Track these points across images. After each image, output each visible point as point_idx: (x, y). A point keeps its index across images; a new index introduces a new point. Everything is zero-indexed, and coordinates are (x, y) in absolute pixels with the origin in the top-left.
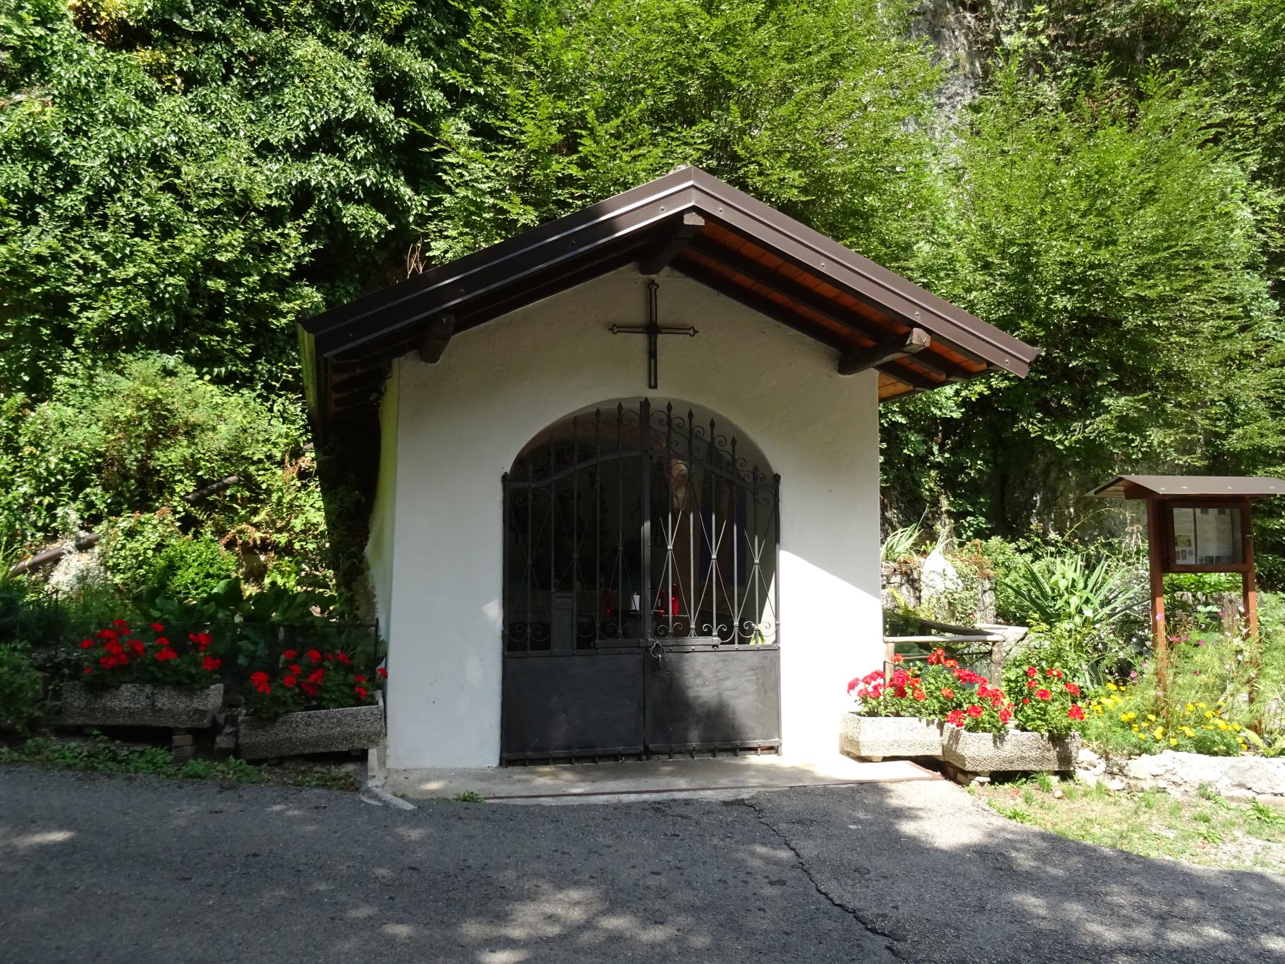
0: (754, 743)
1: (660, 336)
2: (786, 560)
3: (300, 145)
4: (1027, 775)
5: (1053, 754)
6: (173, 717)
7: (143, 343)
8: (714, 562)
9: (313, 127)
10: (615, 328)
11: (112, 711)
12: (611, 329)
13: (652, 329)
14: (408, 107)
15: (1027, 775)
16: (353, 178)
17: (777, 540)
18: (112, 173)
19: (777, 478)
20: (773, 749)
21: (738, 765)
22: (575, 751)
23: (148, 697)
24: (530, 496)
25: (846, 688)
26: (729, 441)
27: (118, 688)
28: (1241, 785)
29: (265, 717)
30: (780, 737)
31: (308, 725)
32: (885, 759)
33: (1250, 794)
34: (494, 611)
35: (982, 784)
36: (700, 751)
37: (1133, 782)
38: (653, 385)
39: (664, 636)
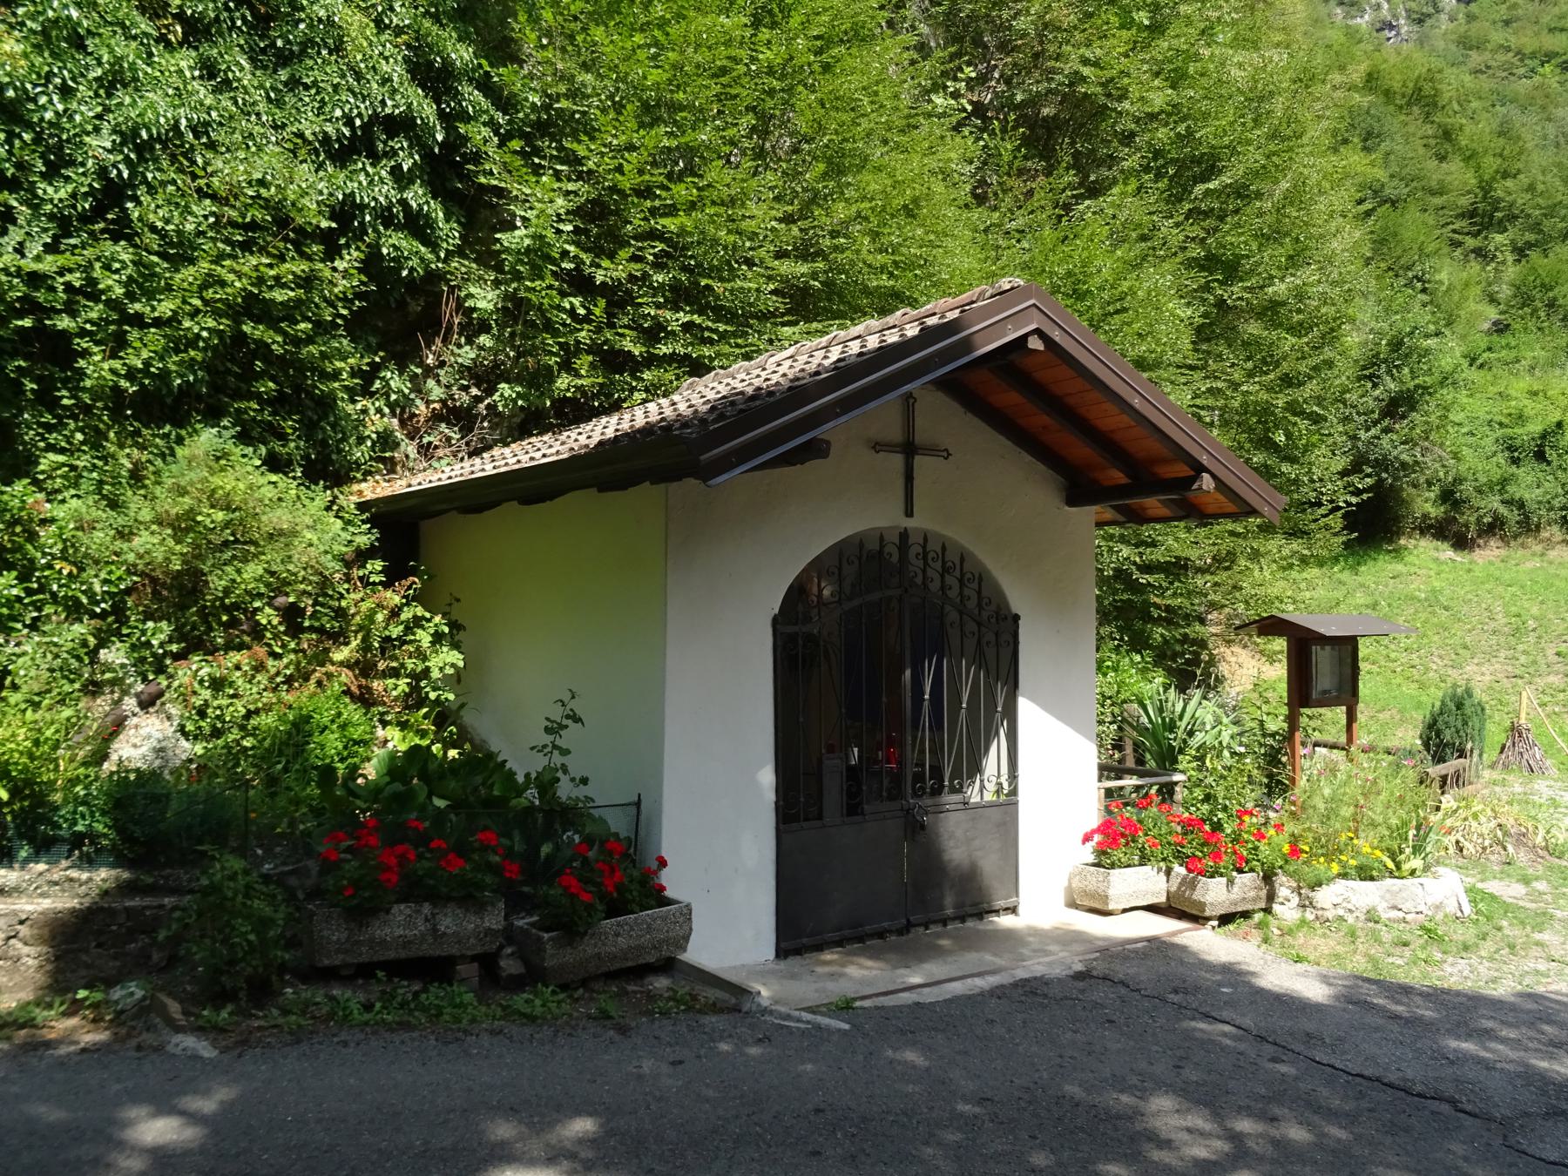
0: (1001, 903)
1: (917, 458)
2: (1026, 708)
3: (341, 144)
4: (1246, 915)
5: (1263, 893)
6: (459, 942)
7: (198, 414)
8: (926, 703)
9: (358, 122)
10: (878, 446)
11: (383, 942)
12: (874, 447)
13: (909, 449)
14: (449, 105)
15: (1246, 915)
16: (394, 196)
17: (1016, 686)
18: (127, 160)
19: (1016, 618)
20: (1013, 910)
21: (978, 931)
22: (847, 932)
23: (427, 920)
24: (800, 642)
25: (1081, 837)
26: (977, 576)
27: (388, 912)
28: (1395, 907)
29: (570, 928)
30: (1017, 896)
31: (617, 935)
32: (1125, 911)
33: (1401, 914)
34: (767, 777)
35: (1213, 928)
36: (954, 919)
37: (1320, 913)
38: (909, 513)
39: (921, 796)
